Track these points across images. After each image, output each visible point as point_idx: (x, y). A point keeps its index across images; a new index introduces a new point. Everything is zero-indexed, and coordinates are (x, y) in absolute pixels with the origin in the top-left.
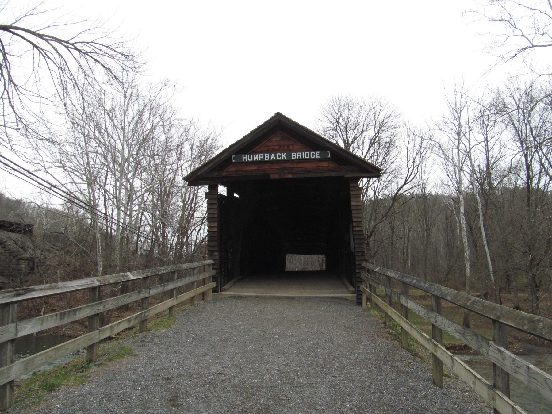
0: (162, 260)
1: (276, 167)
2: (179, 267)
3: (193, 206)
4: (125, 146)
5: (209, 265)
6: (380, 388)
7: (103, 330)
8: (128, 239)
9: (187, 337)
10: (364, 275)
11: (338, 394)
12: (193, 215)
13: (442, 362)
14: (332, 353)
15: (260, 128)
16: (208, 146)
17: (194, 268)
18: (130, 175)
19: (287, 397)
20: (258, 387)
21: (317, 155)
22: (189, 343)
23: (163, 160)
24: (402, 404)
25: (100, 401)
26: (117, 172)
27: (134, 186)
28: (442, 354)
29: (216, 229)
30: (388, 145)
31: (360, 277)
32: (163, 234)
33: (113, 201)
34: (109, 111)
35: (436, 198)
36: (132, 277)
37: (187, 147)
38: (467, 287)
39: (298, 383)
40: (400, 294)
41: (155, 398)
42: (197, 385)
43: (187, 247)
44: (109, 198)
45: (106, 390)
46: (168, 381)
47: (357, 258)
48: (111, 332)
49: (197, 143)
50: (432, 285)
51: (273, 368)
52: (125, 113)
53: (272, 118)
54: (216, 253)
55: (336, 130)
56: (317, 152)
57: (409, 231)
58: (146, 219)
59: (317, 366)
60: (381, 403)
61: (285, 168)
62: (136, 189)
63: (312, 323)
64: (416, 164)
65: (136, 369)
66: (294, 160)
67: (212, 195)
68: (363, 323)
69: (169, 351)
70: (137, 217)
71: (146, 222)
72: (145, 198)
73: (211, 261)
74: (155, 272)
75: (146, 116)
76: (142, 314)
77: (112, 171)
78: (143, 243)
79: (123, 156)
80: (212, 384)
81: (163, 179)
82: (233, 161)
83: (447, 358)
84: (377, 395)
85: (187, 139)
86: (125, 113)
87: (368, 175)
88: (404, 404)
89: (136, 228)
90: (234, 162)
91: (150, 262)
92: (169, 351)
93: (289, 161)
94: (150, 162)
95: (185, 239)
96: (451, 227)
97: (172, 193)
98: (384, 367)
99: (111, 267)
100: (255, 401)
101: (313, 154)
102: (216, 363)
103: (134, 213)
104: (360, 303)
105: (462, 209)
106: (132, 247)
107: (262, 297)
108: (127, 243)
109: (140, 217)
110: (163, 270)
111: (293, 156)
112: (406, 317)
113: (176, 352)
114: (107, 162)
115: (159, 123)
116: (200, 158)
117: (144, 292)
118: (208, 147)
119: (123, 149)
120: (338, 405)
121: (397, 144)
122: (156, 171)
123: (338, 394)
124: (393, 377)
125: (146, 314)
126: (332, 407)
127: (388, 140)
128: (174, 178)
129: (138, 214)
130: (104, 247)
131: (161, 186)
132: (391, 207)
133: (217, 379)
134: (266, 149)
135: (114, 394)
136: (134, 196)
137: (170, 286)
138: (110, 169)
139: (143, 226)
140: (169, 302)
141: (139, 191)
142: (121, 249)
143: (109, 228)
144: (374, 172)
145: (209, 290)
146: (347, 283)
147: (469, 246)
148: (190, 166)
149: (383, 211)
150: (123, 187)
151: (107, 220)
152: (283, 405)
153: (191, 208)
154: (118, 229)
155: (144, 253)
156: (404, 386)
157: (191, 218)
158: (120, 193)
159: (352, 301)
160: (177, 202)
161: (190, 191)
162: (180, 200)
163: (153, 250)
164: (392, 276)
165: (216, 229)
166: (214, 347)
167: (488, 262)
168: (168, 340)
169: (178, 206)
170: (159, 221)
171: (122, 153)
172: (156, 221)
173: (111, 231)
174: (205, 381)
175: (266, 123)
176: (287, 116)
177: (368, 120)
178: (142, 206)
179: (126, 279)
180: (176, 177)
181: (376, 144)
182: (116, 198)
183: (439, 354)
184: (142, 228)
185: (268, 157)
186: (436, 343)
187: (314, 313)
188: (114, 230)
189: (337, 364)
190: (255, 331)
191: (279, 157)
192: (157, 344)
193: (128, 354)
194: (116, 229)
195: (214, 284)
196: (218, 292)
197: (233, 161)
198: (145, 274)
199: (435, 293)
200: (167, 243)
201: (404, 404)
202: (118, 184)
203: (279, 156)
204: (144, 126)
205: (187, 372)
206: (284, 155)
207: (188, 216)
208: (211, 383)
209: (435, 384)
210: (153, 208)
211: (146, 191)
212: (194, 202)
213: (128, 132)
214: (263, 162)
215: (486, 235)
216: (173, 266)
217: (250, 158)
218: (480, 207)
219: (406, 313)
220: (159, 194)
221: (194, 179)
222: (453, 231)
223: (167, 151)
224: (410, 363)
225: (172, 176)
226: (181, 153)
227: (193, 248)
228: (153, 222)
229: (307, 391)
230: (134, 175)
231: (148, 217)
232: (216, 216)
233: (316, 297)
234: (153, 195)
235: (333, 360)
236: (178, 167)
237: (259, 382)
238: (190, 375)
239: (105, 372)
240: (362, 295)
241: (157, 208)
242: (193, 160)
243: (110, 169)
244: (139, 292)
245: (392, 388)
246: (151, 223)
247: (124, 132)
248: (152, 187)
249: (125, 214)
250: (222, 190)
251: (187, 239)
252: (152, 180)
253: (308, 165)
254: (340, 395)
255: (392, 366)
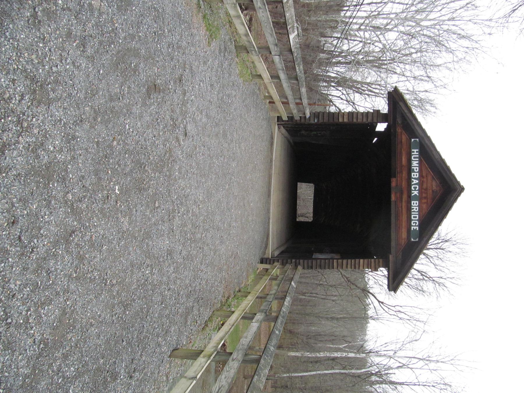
0: (313, 62)
1: (404, 184)
2: (302, 84)
3: (367, 92)
4: (432, 22)
5: (304, 114)
6: (167, 300)
7: (235, 7)
8: (336, 27)
9: (229, 96)
10: (289, 267)
11: (161, 260)
12: (357, 92)
13: (196, 360)
14: (208, 245)
15: (448, 169)
16: (428, 107)
17: (301, 99)
18: (401, 28)
19: (157, 208)
20: (170, 175)
21: (415, 228)
22: (222, 98)
23: (415, 62)
24: (150, 325)
25: (154, 8)
26: (405, 14)
27: (389, 32)
28: (200, 364)
29: (341, 120)
30: (420, 288)
31: (287, 263)
32: (339, 63)
33: (375, 11)
34: (473, 3)
35: (363, 329)
36: (291, 37)
37: (428, 86)
38: (278, 351)
39: (174, 217)
40: (266, 313)
41: (158, 68)
42: (173, 111)
43: (326, 86)
44: (379, 7)
45: (168, 14)
46: (178, 81)
47: (306, 261)
48: (234, 17)
49: (431, 96)
50: (271, 356)
51: (191, 188)
52: (470, 20)
53: (458, 183)
54: (316, 121)
55: (438, 239)
56: (417, 228)
57: (333, 301)
58: (357, 45)
59: (193, 234)
60: (150, 304)
61: (402, 193)
62: (386, 34)
63: (241, 220)
64: (398, 312)
65: (193, 46)
66: (411, 203)
67: (378, 116)
68: (241, 269)
69: (214, 78)
70: (357, 37)
71: (352, 45)
72: (376, 44)
73: (308, 115)
74: (297, 60)
75: (465, 43)
76: (254, 47)
77: (407, 9)
78: (331, 43)
79: (422, 20)
80: (174, 127)
81: (396, 62)
82: (413, 140)
83: (195, 372)
84: (159, 298)
85: (436, 86)
86: (470, 20)
87: (391, 276)
88: (150, 327)
89: (346, 36)
90: (411, 140)
91: (313, 50)
92: (214, 78)
93: (410, 198)
94: (415, 48)
95: (333, 84)
96: (334, 338)
97: (380, 72)
98: (192, 299)
99: (309, 11)
100: (153, 175)
101: (416, 223)
102: (198, 129)
103: (362, 33)
104: (263, 261)
105: (352, 355)
106: (328, 31)
107: (272, 165)
108: (332, 27)
109: (358, 39)
110: (300, 69)
111: (415, 202)
112: (244, 318)
113: (212, 85)
114: (417, 4)
115: (457, 57)
116: (415, 99)
117: (276, 49)
118: (427, 108)
119: (430, 20)
120: (148, 262)
121: (420, 297)
122: (406, 55)
123: (161, 260)
124: (180, 310)
125: (253, 52)
126: (146, 256)
127: (425, 289)
128: (396, 73)
129: (361, 37)
130: (329, 4)
131: (389, 60)
132: (356, 286)
133: (179, 132)
134: (424, 174)
135: (163, 23)
136: (379, 33)
137: (282, 76)
138: (410, 7)
139: (349, 42)
140: (266, 76)
141: (384, 37)
142: (326, 21)
143: (348, 8)
144: (394, 284)
145: (279, 113)
146: (282, 249)
147: (317, 357)
148: (408, 90)
149: (352, 279)
150: (390, 21)
151: (356, 6)
152: (148, 206)
153: (364, 90)
154: (346, 17)
155: (322, 44)
156: (170, 322)
157: (354, 91)
158: (383, 18)
159: (264, 253)
160: (371, 76)
161: (381, 90)
162: (373, 79)
163: (323, 53)
164: (285, 303)
165: (341, 120)
166: (217, 125)
167: (300, 373)
168: (227, 75)
169: (367, 78)
170: (353, 58)
171: (425, 19)
172: (353, 56)
173: (345, 10)
174: (177, 120)
175: (453, 176)
176: (459, 199)
177: (446, 271)
178: (369, 42)
179: (290, 31)
180: (397, 75)
181: (421, 277)
182: (379, 14)
183: (201, 360)
184: (346, 41)
185: (415, 177)
186: (212, 357)
187: (253, 220)
188: (346, 13)
189: (195, 252)
190: (234, 165)
191: (414, 188)
192: (222, 65)
193: (211, 36)
194: (347, 15)
195: (285, 118)
196: (278, 121)
197: (413, 140)
198: (296, 50)
199: (262, 361)
200: (330, 67)
201: (150, 327)
202: (393, 16)
203: (415, 188)
204: (454, 41)
205: (188, 100)
206: (416, 193)
207: (356, 88)
208: (175, 126)
209: (174, 350)
210: (366, 52)
211: (384, 45)
212: (370, 93)
213: (449, 25)
214: (410, 170)
215: (326, 375)
216: (304, 79)
217: (414, 158)
218: (353, 371)
219: (248, 317)
220: (380, 58)
221: (395, 98)
222: (332, 341)
223: (425, 65)
224: (197, 323)
225: (398, 70)
226: (422, 80)
227: (324, 92)
228: (352, 52)
229: (165, 227)
230: (401, 32)
231: (356, 47)
232: (355, 120)
233: (269, 219)
234: (379, 51)
235: (200, 248)
236: (407, 77)
237: (175, 177)
238: (184, 103)
239: (190, 12)
240: (270, 264)
241: (366, 56)
242: (413, 92)
243: (410, 7)
244: (276, 45)
245: (167, 312)
246: (351, 50)
247: (449, 20)
248: (388, 51)
249: (362, 25)
250: (381, 127)
251: (333, 86)
252: (395, 51)
253: (404, 218)
254: (159, 262)
255: (193, 307)
